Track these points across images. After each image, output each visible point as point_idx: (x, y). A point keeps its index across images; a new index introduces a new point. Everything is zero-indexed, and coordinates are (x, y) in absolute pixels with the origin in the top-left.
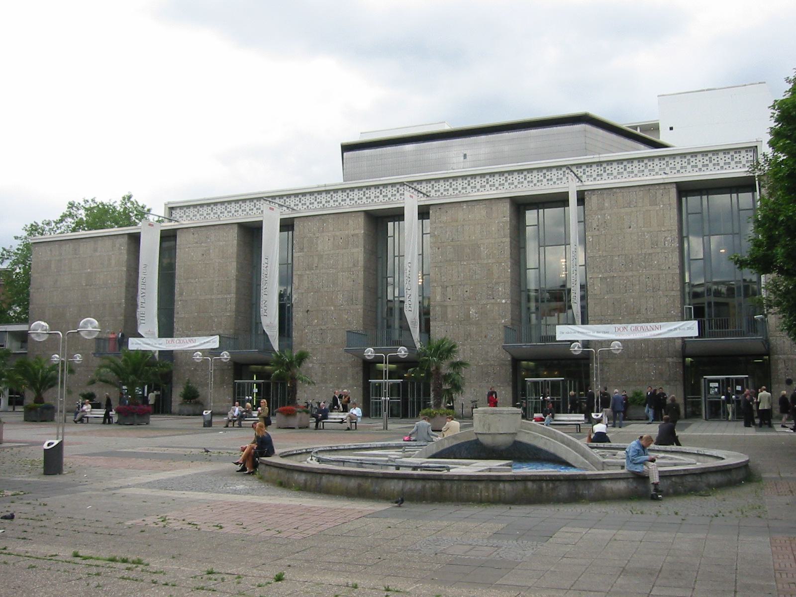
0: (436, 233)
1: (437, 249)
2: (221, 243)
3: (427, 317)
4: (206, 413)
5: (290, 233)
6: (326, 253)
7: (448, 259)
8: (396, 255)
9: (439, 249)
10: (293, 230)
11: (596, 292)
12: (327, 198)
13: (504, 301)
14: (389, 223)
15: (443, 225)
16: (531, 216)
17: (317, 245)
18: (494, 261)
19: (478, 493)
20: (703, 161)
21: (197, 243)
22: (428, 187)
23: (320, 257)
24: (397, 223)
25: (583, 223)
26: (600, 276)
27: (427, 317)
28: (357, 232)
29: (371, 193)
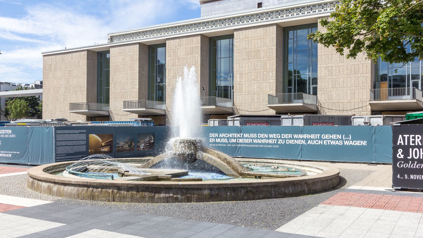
0: (237, 45)
1: (238, 54)
2: (131, 53)
3: (314, 86)
4: (400, 151)
5: (231, 40)
6: (182, 57)
7: (243, 59)
8: (219, 58)
9: (238, 53)
10: (165, 47)
12: (257, 18)
13: (272, 81)
14: (290, 32)
15: (240, 40)
16: (291, 33)
17: (178, 53)
18: (267, 59)
19: (152, 140)
20: (308, 10)
21: (120, 53)
22: (248, 19)
23: (179, 59)
24: (295, 31)
25: (293, 39)
26: (325, 66)
27: (314, 86)
28: (197, 45)
29: (254, 18)
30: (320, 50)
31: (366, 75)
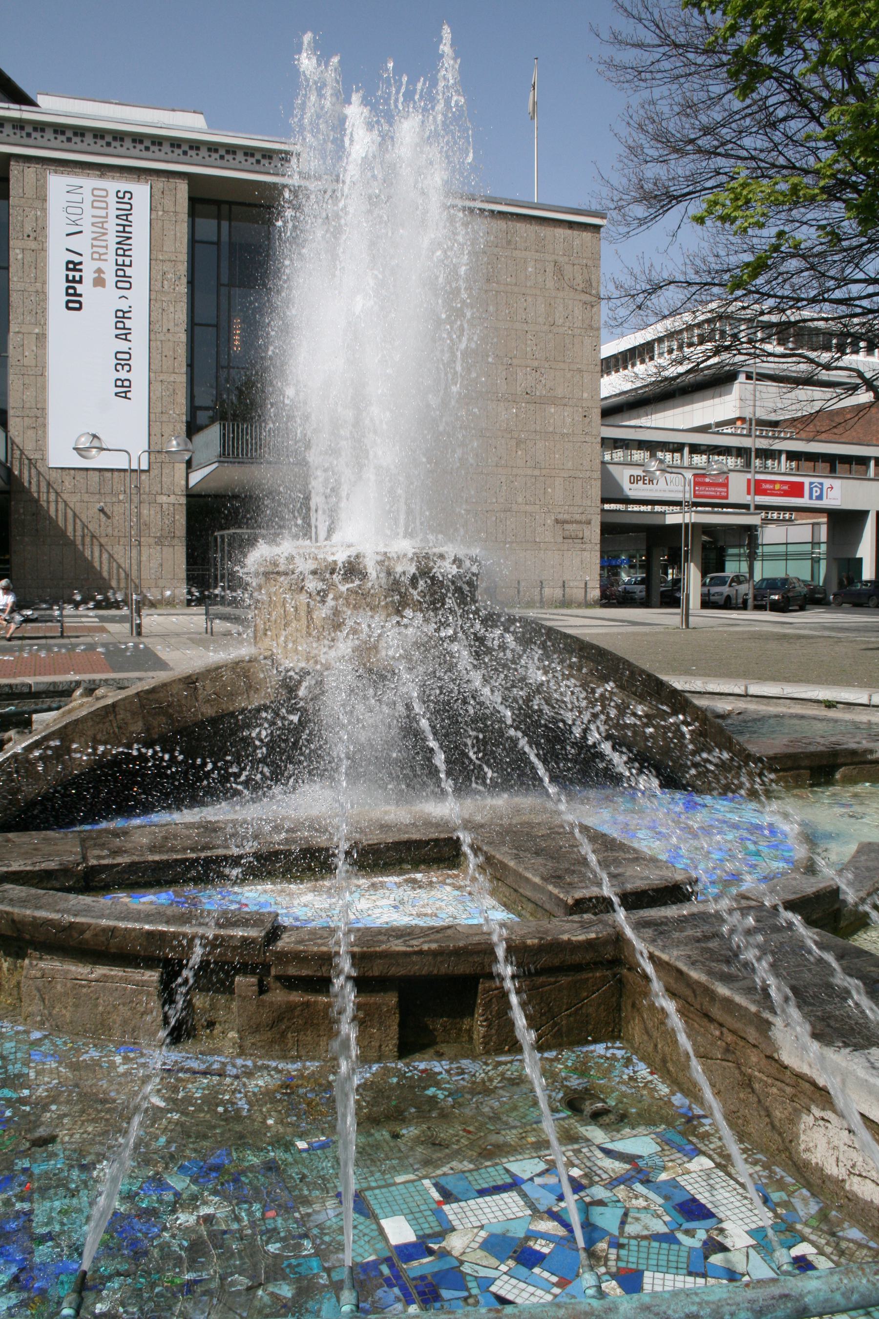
11: (26, 362)
26: (37, 331)
30: (20, 274)
31: (172, 379)
